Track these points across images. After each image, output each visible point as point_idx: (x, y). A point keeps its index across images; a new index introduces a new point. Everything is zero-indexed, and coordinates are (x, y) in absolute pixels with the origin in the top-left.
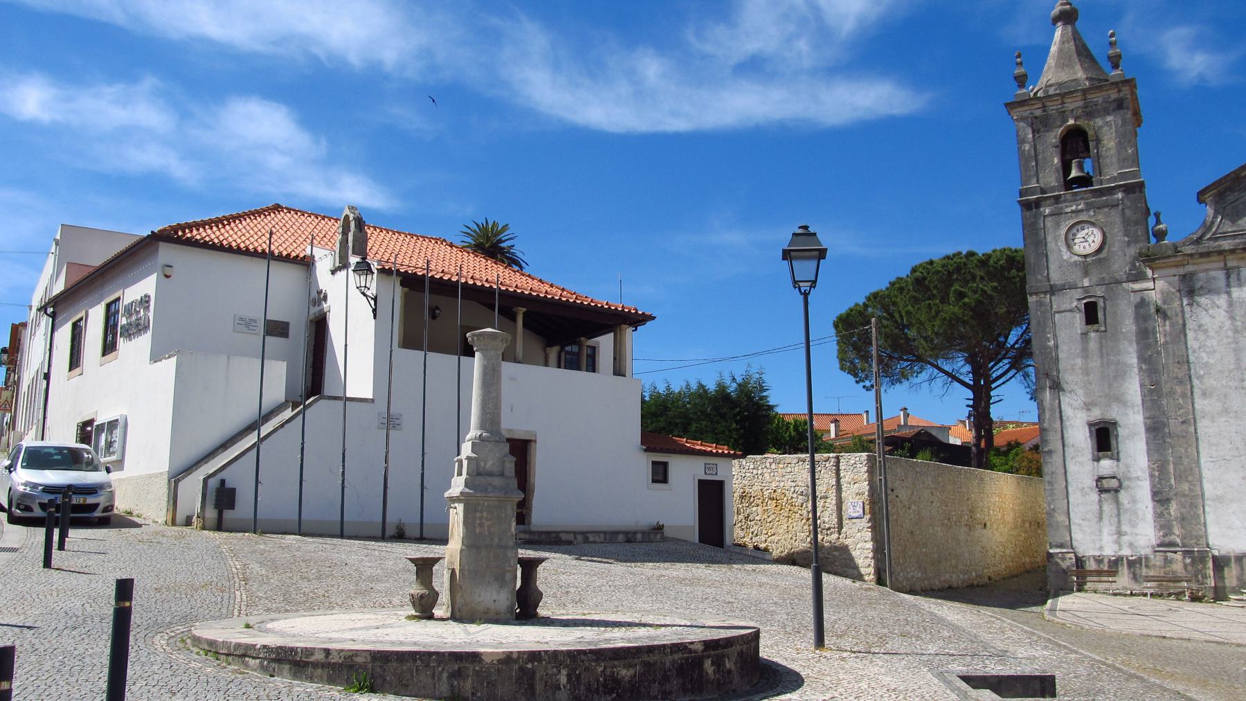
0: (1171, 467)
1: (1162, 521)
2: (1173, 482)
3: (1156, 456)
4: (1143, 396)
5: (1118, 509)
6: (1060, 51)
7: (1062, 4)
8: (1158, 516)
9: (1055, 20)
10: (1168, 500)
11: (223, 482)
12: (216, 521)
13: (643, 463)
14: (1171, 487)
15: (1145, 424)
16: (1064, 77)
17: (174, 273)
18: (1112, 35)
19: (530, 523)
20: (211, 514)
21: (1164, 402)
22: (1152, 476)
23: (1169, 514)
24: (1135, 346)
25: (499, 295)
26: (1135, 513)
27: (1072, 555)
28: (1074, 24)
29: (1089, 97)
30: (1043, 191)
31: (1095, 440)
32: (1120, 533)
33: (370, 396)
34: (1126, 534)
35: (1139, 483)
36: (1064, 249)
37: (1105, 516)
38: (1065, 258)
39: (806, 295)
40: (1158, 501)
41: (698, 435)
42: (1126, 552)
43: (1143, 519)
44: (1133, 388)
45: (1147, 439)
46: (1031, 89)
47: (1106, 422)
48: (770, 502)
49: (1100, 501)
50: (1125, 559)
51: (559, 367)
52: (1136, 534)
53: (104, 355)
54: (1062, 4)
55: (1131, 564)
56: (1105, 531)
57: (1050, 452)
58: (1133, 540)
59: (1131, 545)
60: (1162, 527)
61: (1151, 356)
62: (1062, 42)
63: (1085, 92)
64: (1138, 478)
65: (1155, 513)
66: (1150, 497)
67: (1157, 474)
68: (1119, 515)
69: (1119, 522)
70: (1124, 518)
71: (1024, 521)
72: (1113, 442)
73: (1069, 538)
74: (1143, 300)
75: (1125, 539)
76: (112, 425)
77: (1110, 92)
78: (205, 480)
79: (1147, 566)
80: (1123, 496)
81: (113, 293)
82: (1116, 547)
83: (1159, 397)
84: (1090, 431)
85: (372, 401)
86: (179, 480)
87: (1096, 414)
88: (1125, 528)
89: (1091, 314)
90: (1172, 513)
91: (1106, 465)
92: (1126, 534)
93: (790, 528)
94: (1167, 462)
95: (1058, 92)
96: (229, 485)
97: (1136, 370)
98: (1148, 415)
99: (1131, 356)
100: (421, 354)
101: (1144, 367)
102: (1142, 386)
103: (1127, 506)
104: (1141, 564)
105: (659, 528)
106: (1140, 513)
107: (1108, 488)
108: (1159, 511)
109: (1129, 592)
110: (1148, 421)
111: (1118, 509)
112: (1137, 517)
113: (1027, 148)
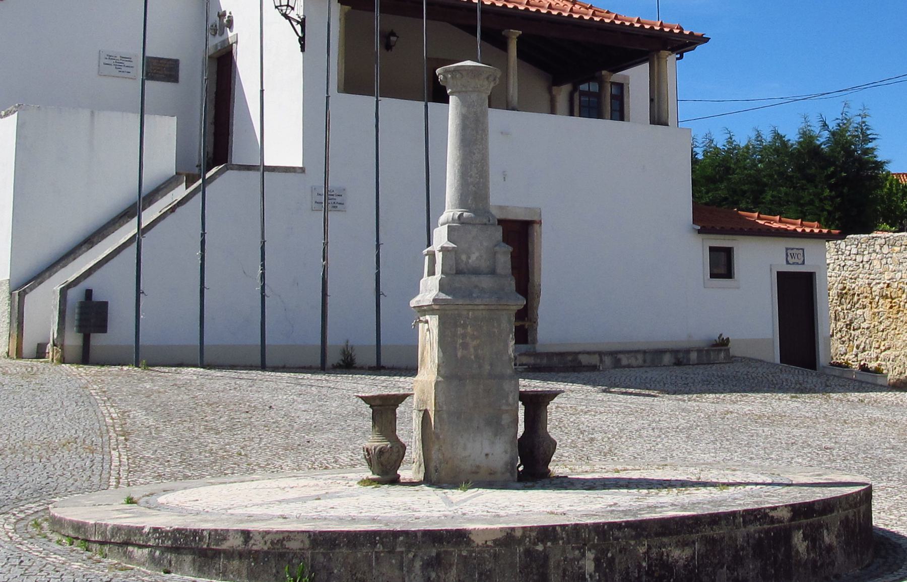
11: (89, 293)
19: (534, 341)
20: (73, 340)
25: (482, 12)
51: (571, 114)
78: (64, 292)
85: (302, 170)
96: (97, 297)
100: (371, 100)
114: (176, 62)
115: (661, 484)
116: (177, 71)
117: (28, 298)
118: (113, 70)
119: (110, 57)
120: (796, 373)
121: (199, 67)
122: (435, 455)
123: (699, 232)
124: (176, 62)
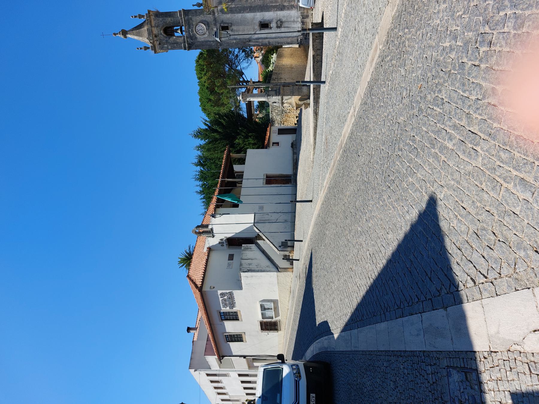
0: (273, 4)
1: (290, 8)
2: (278, 4)
3: (270, 9)
4: (251, 12)
5: (286, 22)
6: (137, 35)
7: (120, 34)
8: (288, 9)
9: (126, 37)
10: (284, 6)
11: (280, 246)
12: (291, 248)
13: (273, 149)
14: (279, 5)
15: (260, 12)
16: (146, 34)
17: (213, 286)
18: (132, 17)
19: (291, 175)
20: (289, 249)
21: (253, 6)
22: (276, 10)
23: (288, 6)
24: (235, 14)
25: (218, 203)
26: (287, 16)
27: (301, 36)
28: (127, 31)
29: (153, 26)
30: (185, 42)
31: (265, 28)
32: (294, 21)
33: (254, 214)
34: (294, 19)
35: (278, 15)
36: (204, 36)
37: (289, 26)
38: (207, 36)
39: (231, 35)
40: (284, 9)
41: (264, 139)
42: (299, 20)
43: (289, 14)
44: (249, 15)
45: (265, 12)
46: (150, 45)
47: (260, 25)
48: (285, 124)
49: (284, 27)
50: (302, 20)
51: (242, 183)
52: (294, 16)
53: (238, 320)
54: (120, 34)
55: (303, 18)
56: (293, 26)
57: (269, 43)
58: (296, 18)
59: (297, 18)
60: (292, 8)
61: (239, 9)
62: (134, 35)
63: (152, 27)
64: (277, 15)
65: (287, 10)
66: (283, 11)
67: (275, 9)
68: (288, 22)
69: (290, 21)
70: (289, 20)
71: (291, 57)
72: (266, 22)
73: (296, 38)
74: (221, 11)
75: (295, 20)
76: (263, 308)
77: (152, 18)
78: (279, 251)
79: (304, 13)
80: (284, 20)
81: (220, 301)
82: (298, 23)
83: (252, 7)
84: (262, 30)
85: (255, 214)
86: (280, 268)
87: (257, 27)
88: (292, 20)
89: (225, 28)
90: (287, 5)
91: (273, 25)
92: (294, 19)
93: (293, 117)
94: (272, 6)
95: (151, 36)
96: (280, 245)
97: (243, 14)
98: (257, 11)
99: (239, 16)
100: (241, 196)
101: (242, 12)
102: (248, 13)
103: (285, 19)
104: (303, 15)
105: (292, 144)
106: (287, 15)
107: (280, 24)
108: (287, 9)
109: (312, 19)
110: (259, 11)
111: (286, 22)
112: (289, 16)
113: (170, 47)
114: (229, 254)
115: (317, 105)
116: (231, 254)
117: (281, 267)
118: (231, 266)
119: (228, 267)
120: (297, 131)
121: (231, 250)
122: (309, 88)
123: (269, 147)
124: (229, 254)
